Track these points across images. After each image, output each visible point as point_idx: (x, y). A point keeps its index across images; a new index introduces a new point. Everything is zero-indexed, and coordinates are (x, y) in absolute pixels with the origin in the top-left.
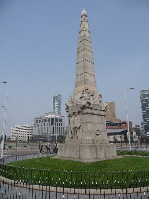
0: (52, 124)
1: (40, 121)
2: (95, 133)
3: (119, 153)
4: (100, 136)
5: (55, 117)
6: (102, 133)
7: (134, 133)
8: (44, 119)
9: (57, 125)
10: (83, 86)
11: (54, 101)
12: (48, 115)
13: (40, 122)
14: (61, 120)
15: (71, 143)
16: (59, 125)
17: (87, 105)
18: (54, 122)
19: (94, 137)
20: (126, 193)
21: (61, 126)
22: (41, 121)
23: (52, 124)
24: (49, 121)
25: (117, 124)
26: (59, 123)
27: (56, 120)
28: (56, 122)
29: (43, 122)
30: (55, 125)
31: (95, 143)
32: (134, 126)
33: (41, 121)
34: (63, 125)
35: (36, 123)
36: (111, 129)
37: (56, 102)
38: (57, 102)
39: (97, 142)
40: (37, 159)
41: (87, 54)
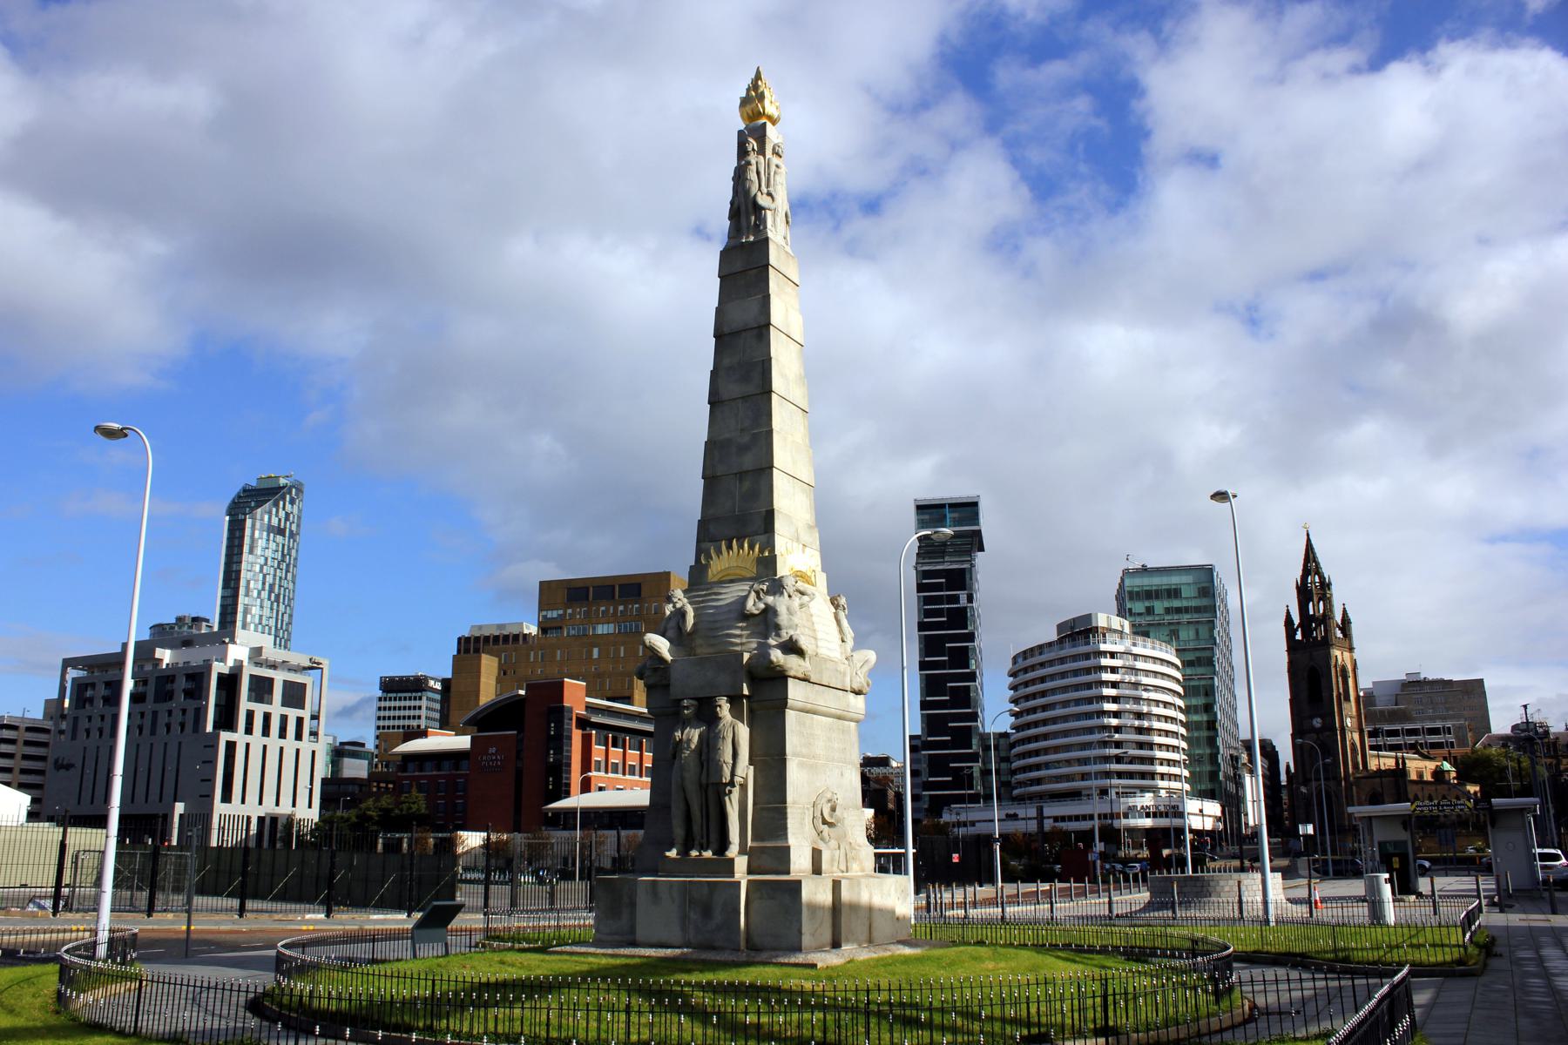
9: (283, 735)
14: (295, 695)
18: (244, 704)
20: (492, 887)
26: (284, 719)
28: (259, 709)
40: (43, 944)
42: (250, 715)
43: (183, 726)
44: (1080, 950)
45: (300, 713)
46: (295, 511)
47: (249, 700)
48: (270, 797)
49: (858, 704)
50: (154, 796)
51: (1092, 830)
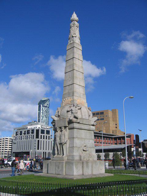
0: (37, 137)
1: (21, 132)
2: (82, 149)
3: (107, 171)
4: (87, 152)
5: (40, 128)
6: (90, 149)
7: (140, 149)
8: (26, 130)
9: (46, 139)
10: (71, 99)
11: (40, 107)
12: (31, 125)
13: (21, 134)
15: (57, 160)
16: (44, 139)
17: (75, 120)
18: (40, 134)
19: (81, 153)
21: (49, 139)
22: (23, 132)
23: (37, 137)
24: (33, 133)
25: (120, 138)
26: (46, 136)
27: (43, 132)
28: (43, 135)
29: (25, 134)
30: (41, 138)
31: (82, 159)
32: (141, 140)
33: (23, 132)
34: (51, 138)
35: (16, 135)
36: (109, 144)
37: (42, 108)
38: (44, 109)
39: (84, 158)
41: (77, 63)
42: (41, 136)
43: (20, 139)
44: (69, 175)
45: (49, 135)
46: (48, 103)
47: (41, 133)
48: (22, 149)
49: (93, 128)
50: (28, 149)
51: (125, 148)
